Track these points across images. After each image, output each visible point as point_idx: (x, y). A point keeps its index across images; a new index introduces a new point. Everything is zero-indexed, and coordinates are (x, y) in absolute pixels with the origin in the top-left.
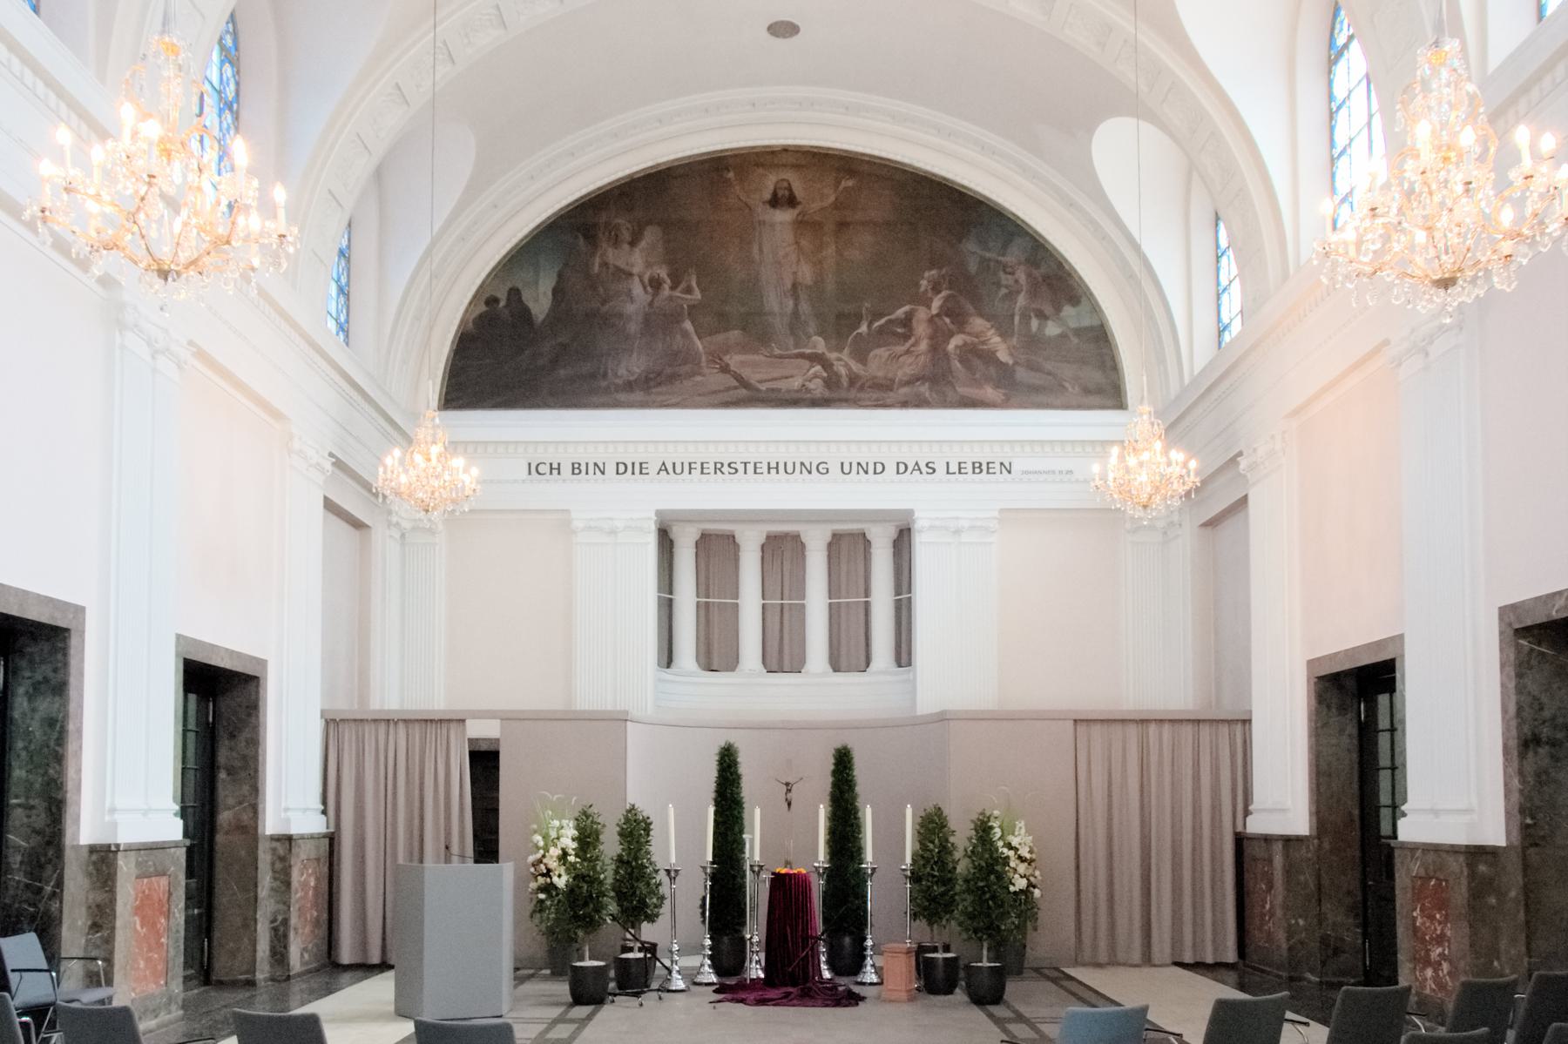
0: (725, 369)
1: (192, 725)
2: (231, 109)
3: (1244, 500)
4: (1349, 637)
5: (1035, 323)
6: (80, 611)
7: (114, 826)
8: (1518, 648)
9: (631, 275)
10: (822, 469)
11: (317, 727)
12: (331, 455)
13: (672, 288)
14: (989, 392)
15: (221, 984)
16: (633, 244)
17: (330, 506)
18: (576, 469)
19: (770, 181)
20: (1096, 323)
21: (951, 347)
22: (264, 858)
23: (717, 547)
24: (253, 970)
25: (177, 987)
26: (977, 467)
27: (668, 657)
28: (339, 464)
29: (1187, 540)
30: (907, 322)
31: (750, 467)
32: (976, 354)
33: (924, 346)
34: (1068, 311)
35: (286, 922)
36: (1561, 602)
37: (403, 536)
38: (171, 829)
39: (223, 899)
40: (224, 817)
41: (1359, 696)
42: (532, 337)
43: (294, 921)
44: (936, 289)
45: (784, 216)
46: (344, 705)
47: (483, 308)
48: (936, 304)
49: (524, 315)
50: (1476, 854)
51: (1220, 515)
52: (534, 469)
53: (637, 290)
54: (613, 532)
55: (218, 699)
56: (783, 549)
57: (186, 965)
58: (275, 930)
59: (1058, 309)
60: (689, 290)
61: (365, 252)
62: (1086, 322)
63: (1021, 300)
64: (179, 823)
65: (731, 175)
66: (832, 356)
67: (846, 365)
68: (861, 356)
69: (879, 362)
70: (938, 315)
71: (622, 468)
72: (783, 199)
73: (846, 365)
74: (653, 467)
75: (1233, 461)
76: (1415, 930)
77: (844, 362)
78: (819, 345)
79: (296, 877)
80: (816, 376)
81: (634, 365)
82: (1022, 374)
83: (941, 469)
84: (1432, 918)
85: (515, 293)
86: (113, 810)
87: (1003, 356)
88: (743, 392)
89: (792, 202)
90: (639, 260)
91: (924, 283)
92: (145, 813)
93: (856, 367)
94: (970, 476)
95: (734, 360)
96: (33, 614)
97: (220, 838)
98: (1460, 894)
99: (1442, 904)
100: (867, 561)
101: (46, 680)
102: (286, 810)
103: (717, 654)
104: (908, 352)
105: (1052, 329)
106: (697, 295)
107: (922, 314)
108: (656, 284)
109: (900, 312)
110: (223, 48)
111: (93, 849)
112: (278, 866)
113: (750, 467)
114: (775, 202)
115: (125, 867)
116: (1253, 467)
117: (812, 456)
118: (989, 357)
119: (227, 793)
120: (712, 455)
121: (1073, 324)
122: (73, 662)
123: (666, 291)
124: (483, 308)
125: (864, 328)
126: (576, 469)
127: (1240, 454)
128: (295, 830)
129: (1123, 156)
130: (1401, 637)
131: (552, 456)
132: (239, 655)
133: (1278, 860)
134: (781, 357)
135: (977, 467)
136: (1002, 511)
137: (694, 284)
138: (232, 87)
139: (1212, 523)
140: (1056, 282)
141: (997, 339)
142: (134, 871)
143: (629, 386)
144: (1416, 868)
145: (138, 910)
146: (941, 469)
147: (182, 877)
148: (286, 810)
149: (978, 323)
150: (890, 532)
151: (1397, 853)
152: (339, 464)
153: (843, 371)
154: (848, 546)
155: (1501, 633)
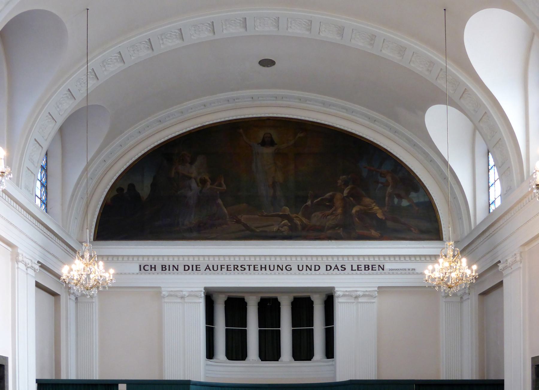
0: (238, 222)
3: (501, 284)
5: (396, 200)
9: (190, 178)
10: (288, 268)
14: (373, 233)
16: (191, 163)
17: (38, 285)
18: (164, 268)
19: (261, 134)
21: (354, 211)
23: (236, 305)
26: (367, 267)
27: (210, 354)
28: (42, 266)
29: (471, 304)
30: (331, 199)
31: (252, 268)
32: (366, 214)
33: (339, 211)
34: (413, 195)
37: (76, 299)
42: (147, 201)
44: (346, 184)
45: (268, 151)
46: (48, 376)
48: (346, 192)
49: (137, 196)
51: (488, 290)
52: (142, 268)
53: (194, 185)
56: (269, 306)
60: (220, 185)
62: (422, 200)
63: (389, 190)
65: (241, 131)
67: (301, 220)
68: (308, 216)
69: (316, 219)
71: (187, 268)
72: (267, 142)
73: (301, 220)
74: (203, 268)
75: (496, 265)
77: (299, 219)
78: (287, 210)
80: (285, 225)
81: (192, 219)
82: (389, 224)
83: (348, 268)
85: (132, 187)
87: (380, 215)
88: (248, 232)
89: (272, 143)
90: (195, 170)
91: (340, 181)
93: (304, 220)
94: (363, 271)
95: (243, 218)
103: (237, 351)
104: (332, 214)
105: (405, 203)
106: (224, 187)
107: (338, 196)
108: (203, 182)
109: (328, 195)
113: (252, 268)
114: (264, 143)
116: (505, 268)
117: (283, 262)
118: (373, 216)
120: (232, 262)
121: (415, 201)
123: (209, 186)
125: (309, 203)
126: (164, 268)
127: (499, 262)
129: (442, 125)
131: (151, 262)
134: (266, 216)
135: (367, 267)
136: (379, 287)
137: (223, 182)
139: (485, 294)
141: (377, 208)
146: (348, 268)
149: (367, 200)
150: (324, 297)
152: (42, 266)
153: (298, 222)
154: (302, 305)
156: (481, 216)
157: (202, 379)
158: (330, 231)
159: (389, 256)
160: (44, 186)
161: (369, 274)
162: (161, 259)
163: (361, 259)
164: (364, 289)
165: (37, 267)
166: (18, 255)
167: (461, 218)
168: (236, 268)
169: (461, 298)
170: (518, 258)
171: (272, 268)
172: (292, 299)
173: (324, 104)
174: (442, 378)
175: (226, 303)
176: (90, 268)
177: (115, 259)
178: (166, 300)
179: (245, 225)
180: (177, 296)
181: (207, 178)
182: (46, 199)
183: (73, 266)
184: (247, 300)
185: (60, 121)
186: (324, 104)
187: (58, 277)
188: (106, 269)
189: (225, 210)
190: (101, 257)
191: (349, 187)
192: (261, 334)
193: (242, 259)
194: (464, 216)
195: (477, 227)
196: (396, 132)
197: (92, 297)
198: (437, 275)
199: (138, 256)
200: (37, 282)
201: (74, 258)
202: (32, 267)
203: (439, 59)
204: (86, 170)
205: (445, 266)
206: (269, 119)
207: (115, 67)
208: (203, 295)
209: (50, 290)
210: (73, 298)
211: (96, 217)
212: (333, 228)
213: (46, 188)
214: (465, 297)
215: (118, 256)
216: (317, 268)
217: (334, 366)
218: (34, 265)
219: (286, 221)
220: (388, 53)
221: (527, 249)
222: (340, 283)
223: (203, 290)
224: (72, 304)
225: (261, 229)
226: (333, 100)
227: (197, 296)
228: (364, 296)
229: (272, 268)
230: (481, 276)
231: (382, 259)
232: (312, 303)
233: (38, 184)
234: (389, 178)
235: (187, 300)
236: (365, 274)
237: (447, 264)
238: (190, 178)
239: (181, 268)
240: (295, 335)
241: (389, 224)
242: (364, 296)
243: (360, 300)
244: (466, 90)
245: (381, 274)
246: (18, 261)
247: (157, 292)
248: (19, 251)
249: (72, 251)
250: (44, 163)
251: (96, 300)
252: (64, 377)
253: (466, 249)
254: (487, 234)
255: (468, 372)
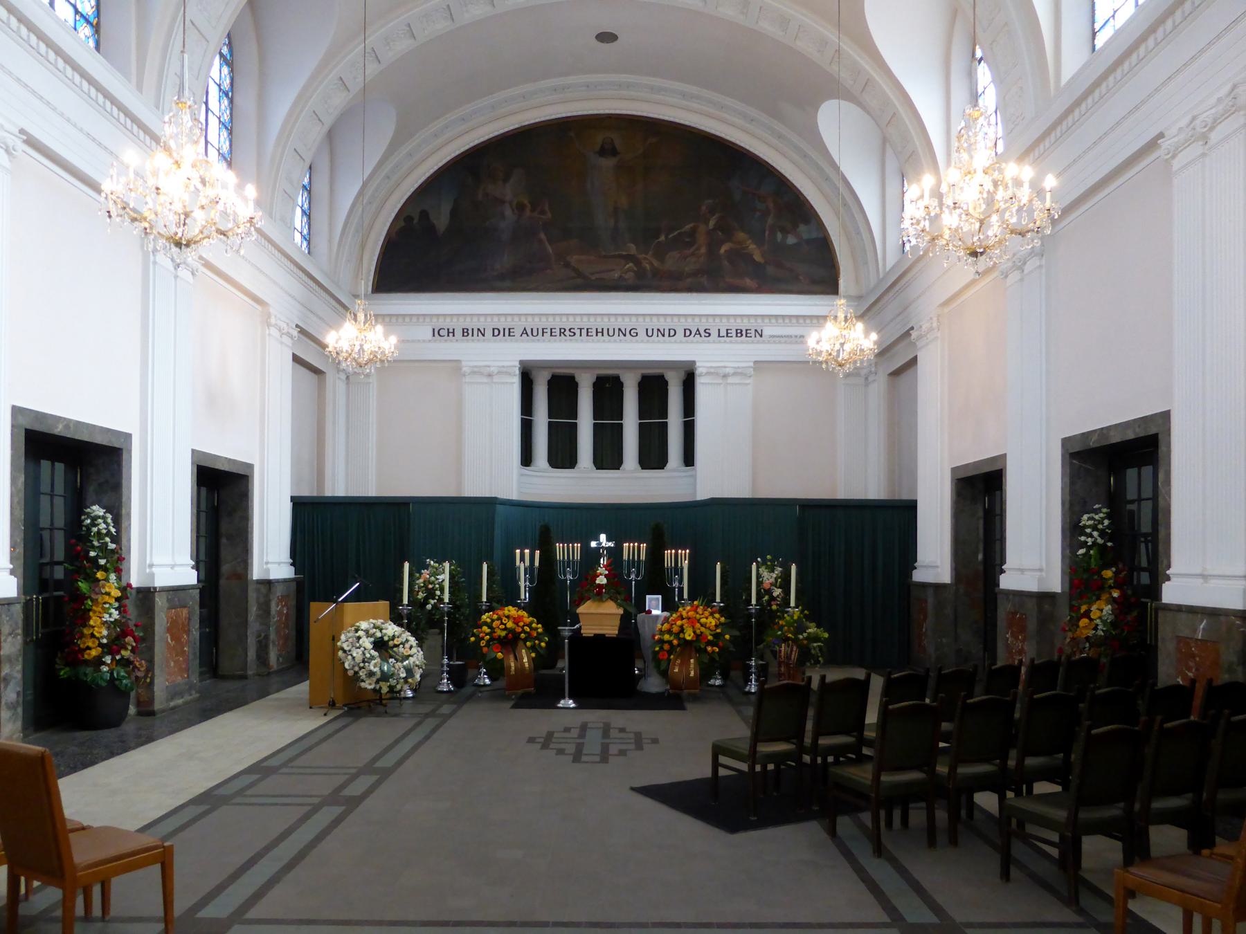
0: (567, 265)
1: (203, 507)
2: (227, 95)
3: (914, 361)
4: (975, 453)
5: (779, 236)
6: (128, 437)
7: (152, 575)
8: (1071, 464)
9: (503, 202)
10: (633, 333)
11: (288, 506)
12: (297, 326)
13: (533, 210)
14: (748, 282)
15: (224, 678)
16: (506, 180)
17: (296, 359)
18: (465, 332)
19: (599, 138)
20: (821, 235)
21: (722, 251)
22: (252, 595)
23: (563, 386)
24: (245, 668)
25: (195, 679)
26: (739, 333)
27: (527, 459)
28: (303, 332)
29: (880, 384)
30: (693, 233)
31: (584, 332)
32: (739, 256)
33: (703, 250)
34: (802, 228)
35: (267, 637)
36: (1095, 438)
37: (348, 378)
38: (188, 576)
39: (224, 622)
40: (225, 568)
41: (981, 490)
42: (446, 236)
43: (273, 636)
44: (712, 212)
45: (608, 163)
46: (306, 492)
47: (403, 224)
48: (712, 223)
49: (430, 229)
50: (1044, 598)
51: (898, 366)
52: (437, 333)
53: (508, 212)
54: (490, 375)
55: (221, 492)
56: (608, 388)
57: (201, 665)
58: (260, 642)
59: (795, 226)
60: (543, 212)
61: (321, 187)
62: (814, 235)
63: (770, 220)
64: (195, 573)
65: (572, 134)
66: (641, 256)
67: (651, 264)
68: (660, 255)
69: (672, 261)
70: (714, 229)
71: (496, 332)
72: (607, 150)
73: (651, 264)
74: (518, 332)
75: (907, 334)
76: (1007, 646)
77: (649, 261)
78: (632, 248)
79: (274, 608)
80: (629, 270)
81: (506, 261)
82: (771, 270)
83: (714, 333)
84: (1017, 638)
85: (424, 215)
86: (151, 566)
87: (758, 257)
88: (579, 281)
89: (614, 152)
90: (509, 191)
91: (704, 208)
92: (173, 566)
93: (656, 263)
94: (734, 338)
95: (574, 259)
96: (99, 439)
97: (223, 582)
98: (1032, 625)
99: (1023, 629)
100: (655, 404)
101: (107, 482)
102: (267, 563)
103: (563, 456)
104: (693, 254)
105: (791, 240)
106: (549, 215)
107: (702, 228)
108: (520, 208)
109: (688, 227)
110: (221, 55)
111: (139, 590)
112: (262, 600)
113: (584, 332)
114: (603, 152)
115: (160, 601)
116: (920, 337)
117: (626, 324)
118: (749, 258)
119: (225, 552)
120: (558, 324)
121: (805, 236)
122: (124, 470)
123: (528, 213)
124: (403, 224)
125: (662, 238)
126: (465, 332)
127: (912, 328)
128: (273, 576)
129: (837, 125)
130: (1004, 456)
131: (448, 324)
132: (234, 461)
133: (930, 600)
134: (605, 257)
135: (739, 333)
136: (755, 362)
137: (547, 208)
138: (228, 81)
139: (896, 373)
140: (796, 209)
141: (752, 246)
142: (166, 605)
143: (502, 277)
144: (1009, 607)
145: (169, 630)
146: (714, 333)
147: (197, 608)
148: (267, 563)
149: (741, 235)
150: (682, 376)
151: (999, 597)
152: (303, 332)
153: (648, 266)
154: (653, 386)
155: (1063, 456)
156: (892, 259)
157: (514, 496)
158: (689, 280)
159: (770, 317)
160: (307, 214)
161: (742, 342)
162: (461, 319)
163: (732, 320)
164: (736, 365)
165: (295, 333)
166: (269, 316)
167: (866, 263)
168: (562, 332)
169: (866, 379)
170: (935, 325)
171: (611, 333)
172: (639, 378)
173: (684, 95)
174: (839, 497)
175: (549, 382)
176: (364, 335)
177: (400, 320)
178: (467, 379)
179: (575, 270)
180: (481, 374)
181: (526, 202)
182: (309, 233)
183: (342, 331)
184: (577, 379)
185: (328, 121)
186: (684, 95)
187: (324, 346)
188: (386, 336)
189: (550, 249)
190: (379, 318)
191: (717, 215)
192: (597, 429)
193: (571, 319)
194: (870, 255)
195: (887, 274)
196: (780, 137)
197: (368, 375)
198: (825, 347)
199: (431, 316)
200: (294, 355)
201: (344, 318)
202: (288, 334)
203: (831, 35)
204: (361, 193)
205: (837, 333)
206: (610, 117)
207: (403, 45)
208: (517, 372)
209: (311, 367)
210: (343, 377)
211: (376, 258)
212: (695, 274)
213: (309, 217)
214: (870, 379)
215: (404, 316)
216: (672, 333)
217: (694, 477)
218: (291, 331)
219: (631, 264)
220: (766, 27)
221: (946, 310)
222: (704, 356)
223: (517, 364)
224: (341, 386)
225: (597, 276)
226: (694, 89)
227: (509, 374)
228: (735, 374)
229: (611, 333)
230: (884, 352)
231: (759, 321)
232: (666, 383)
233: (299, 211)
234: (771, 205)
235: (496, 379)
236: (736, 342)
237: (990, 233)
238: (503, 202)
239: (489, 333)
240: (643, 430)
241: (771, 270)
242: (735, 374)
243: (730, 380)
244: (869, 82)
245: (758, 342)
246: (269, 325)
247: (455, 367)
248: (271, 310)
249: (343, 309)
250: (306, 181)
251: (373, 380)
252: (328, 493)
253: (868, 312)
254: (897, 287)
255: (873, 489)
